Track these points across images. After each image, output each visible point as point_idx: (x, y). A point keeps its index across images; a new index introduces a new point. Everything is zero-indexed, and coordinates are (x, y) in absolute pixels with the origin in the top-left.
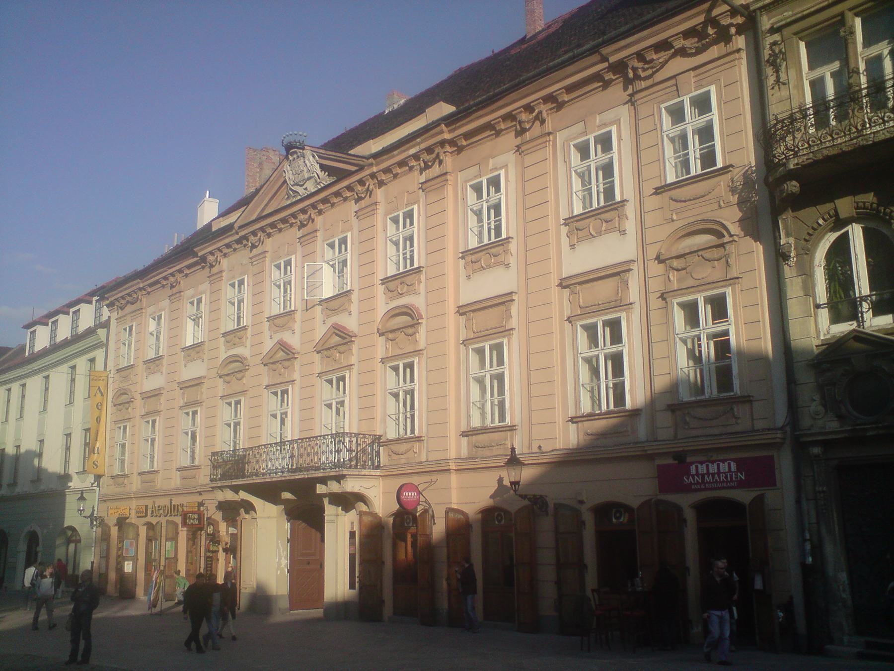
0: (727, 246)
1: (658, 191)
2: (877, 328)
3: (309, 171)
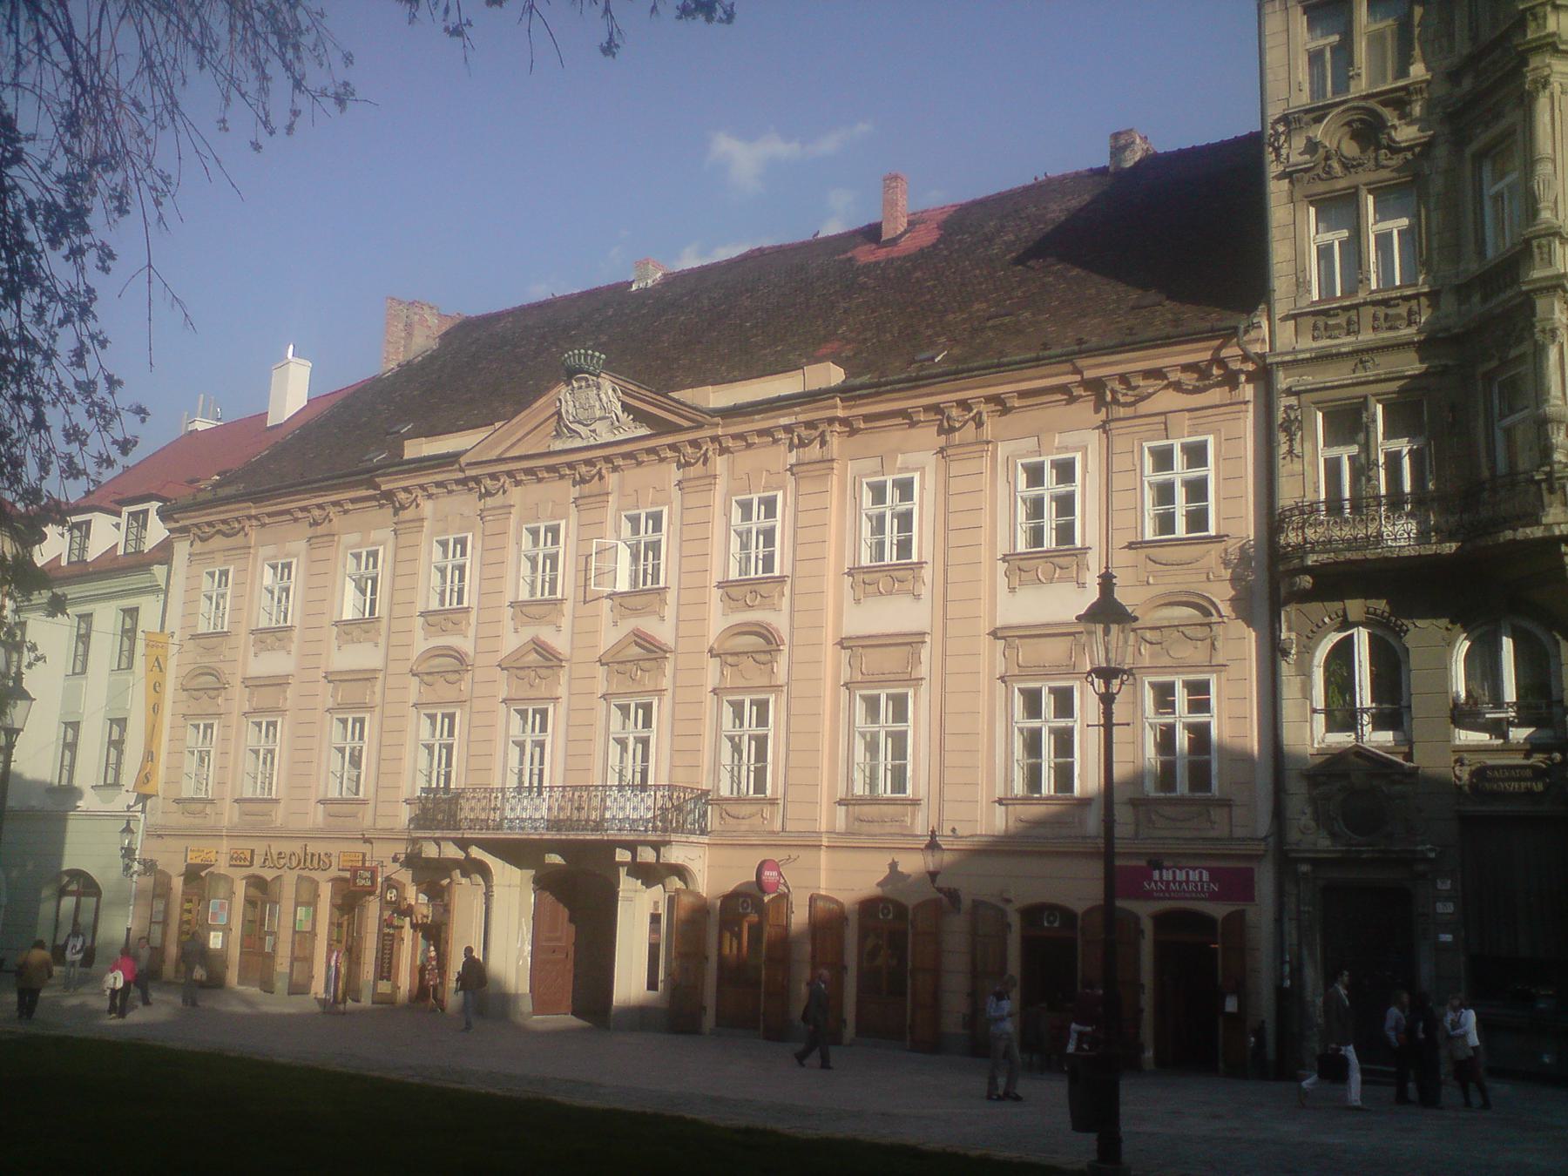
0: (1214, 627)
1: (1131, 546)
2: (1375, 745)
3: (603, 408)
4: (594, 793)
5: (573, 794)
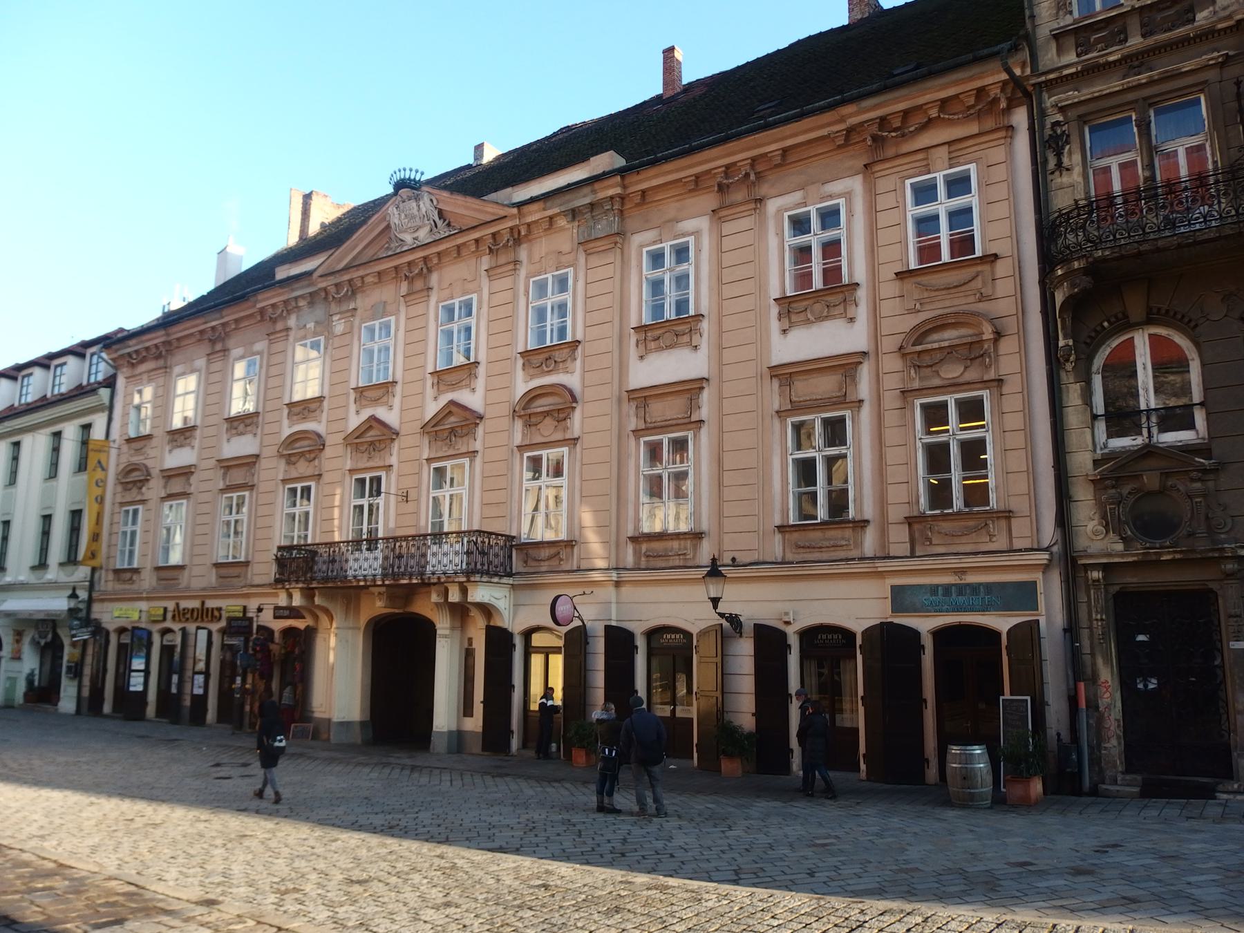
4: (412, 543)
5: (395, 545)
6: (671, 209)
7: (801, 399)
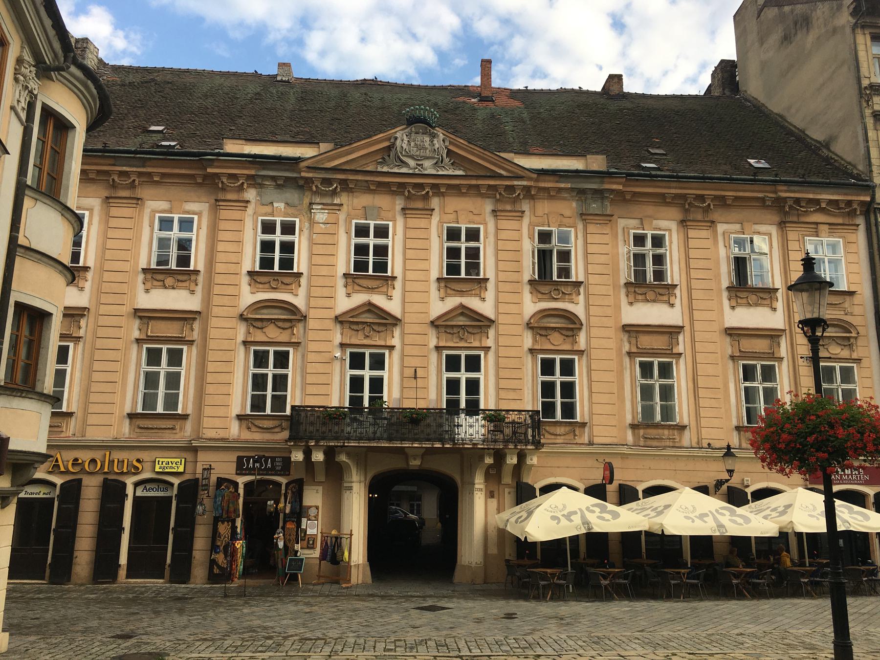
6: (650, 210)
7: (747, 351)
